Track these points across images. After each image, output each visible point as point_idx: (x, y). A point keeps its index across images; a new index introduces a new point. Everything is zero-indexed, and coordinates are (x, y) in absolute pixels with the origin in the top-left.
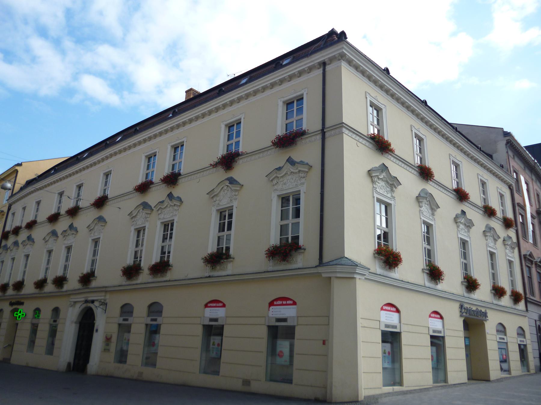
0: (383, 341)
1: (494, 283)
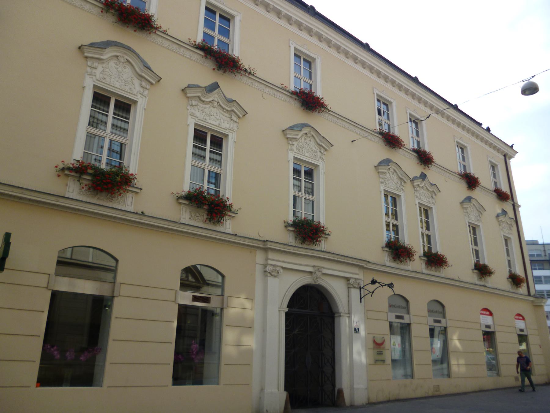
0: (484, 341)
1: (510, 271)
